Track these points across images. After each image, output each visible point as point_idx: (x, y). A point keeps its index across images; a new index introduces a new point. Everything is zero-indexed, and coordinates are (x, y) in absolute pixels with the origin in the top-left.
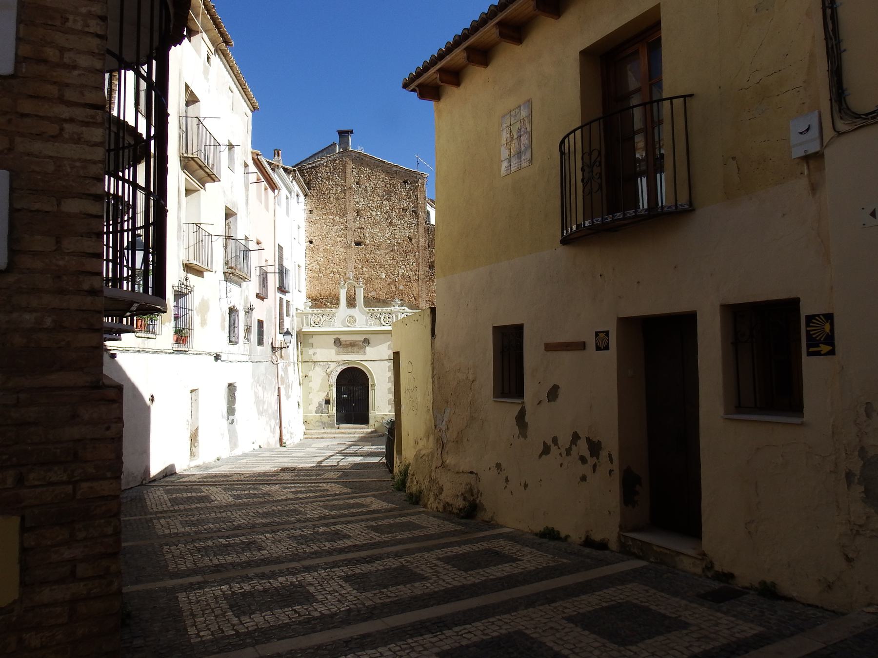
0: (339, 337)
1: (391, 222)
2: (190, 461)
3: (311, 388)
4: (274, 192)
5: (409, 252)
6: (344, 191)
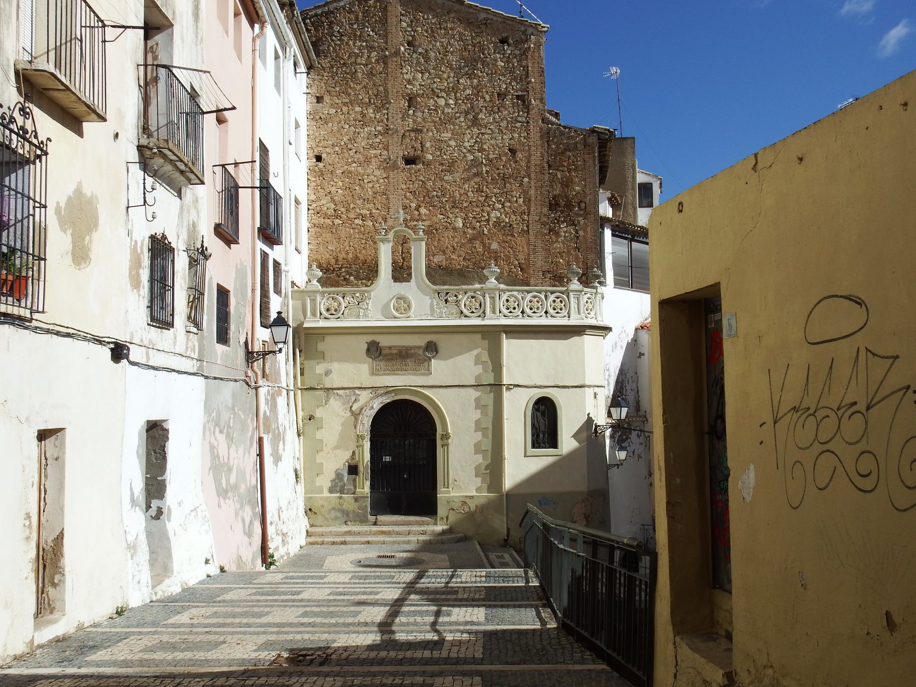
0: (377, 338)
1: (475, 118)
2: (37, 627)
3: (321, 441)
4: (252, 27)
5: (511, 176)
6: (384, 60)
